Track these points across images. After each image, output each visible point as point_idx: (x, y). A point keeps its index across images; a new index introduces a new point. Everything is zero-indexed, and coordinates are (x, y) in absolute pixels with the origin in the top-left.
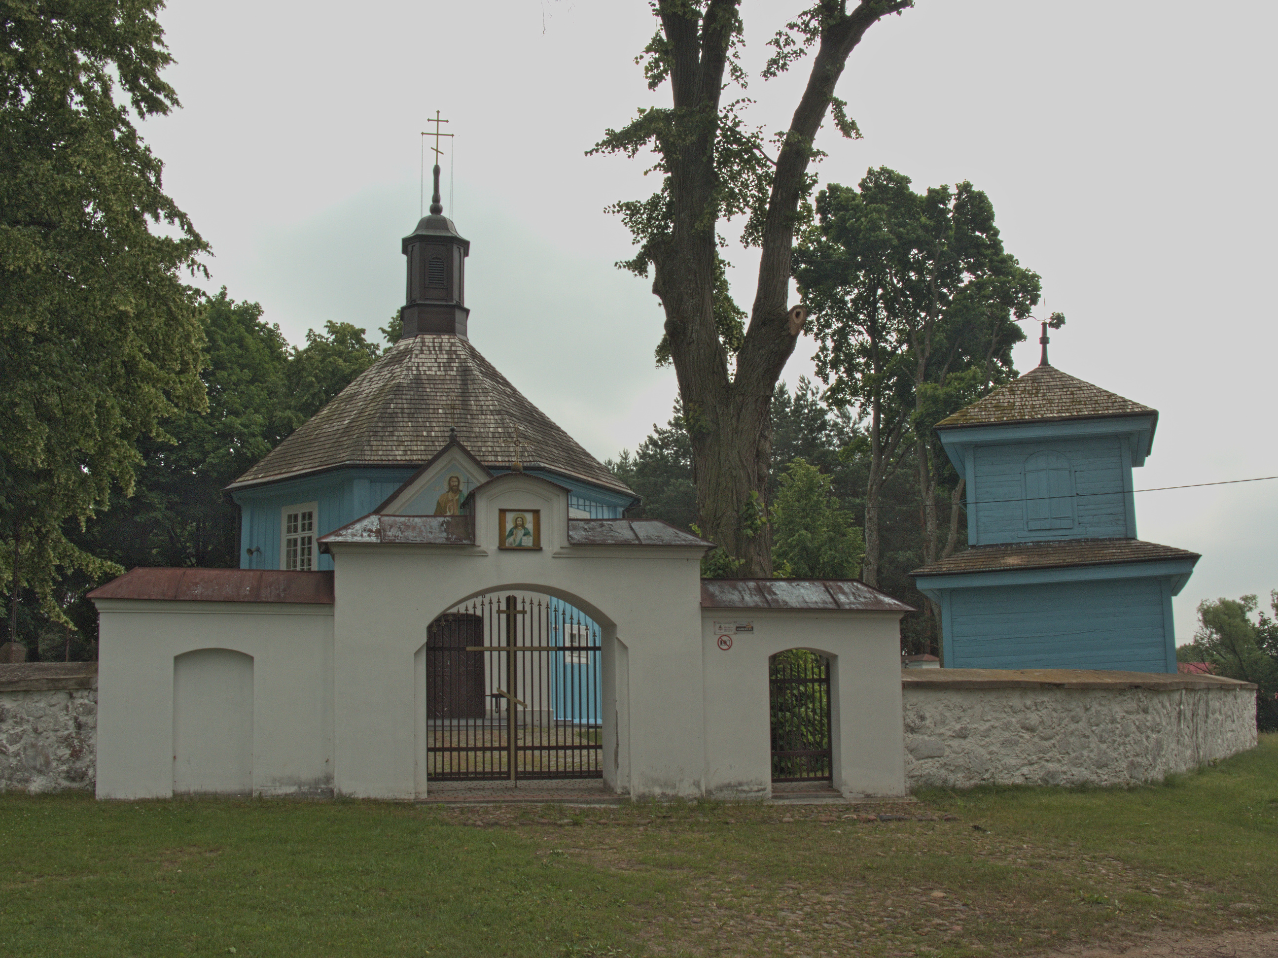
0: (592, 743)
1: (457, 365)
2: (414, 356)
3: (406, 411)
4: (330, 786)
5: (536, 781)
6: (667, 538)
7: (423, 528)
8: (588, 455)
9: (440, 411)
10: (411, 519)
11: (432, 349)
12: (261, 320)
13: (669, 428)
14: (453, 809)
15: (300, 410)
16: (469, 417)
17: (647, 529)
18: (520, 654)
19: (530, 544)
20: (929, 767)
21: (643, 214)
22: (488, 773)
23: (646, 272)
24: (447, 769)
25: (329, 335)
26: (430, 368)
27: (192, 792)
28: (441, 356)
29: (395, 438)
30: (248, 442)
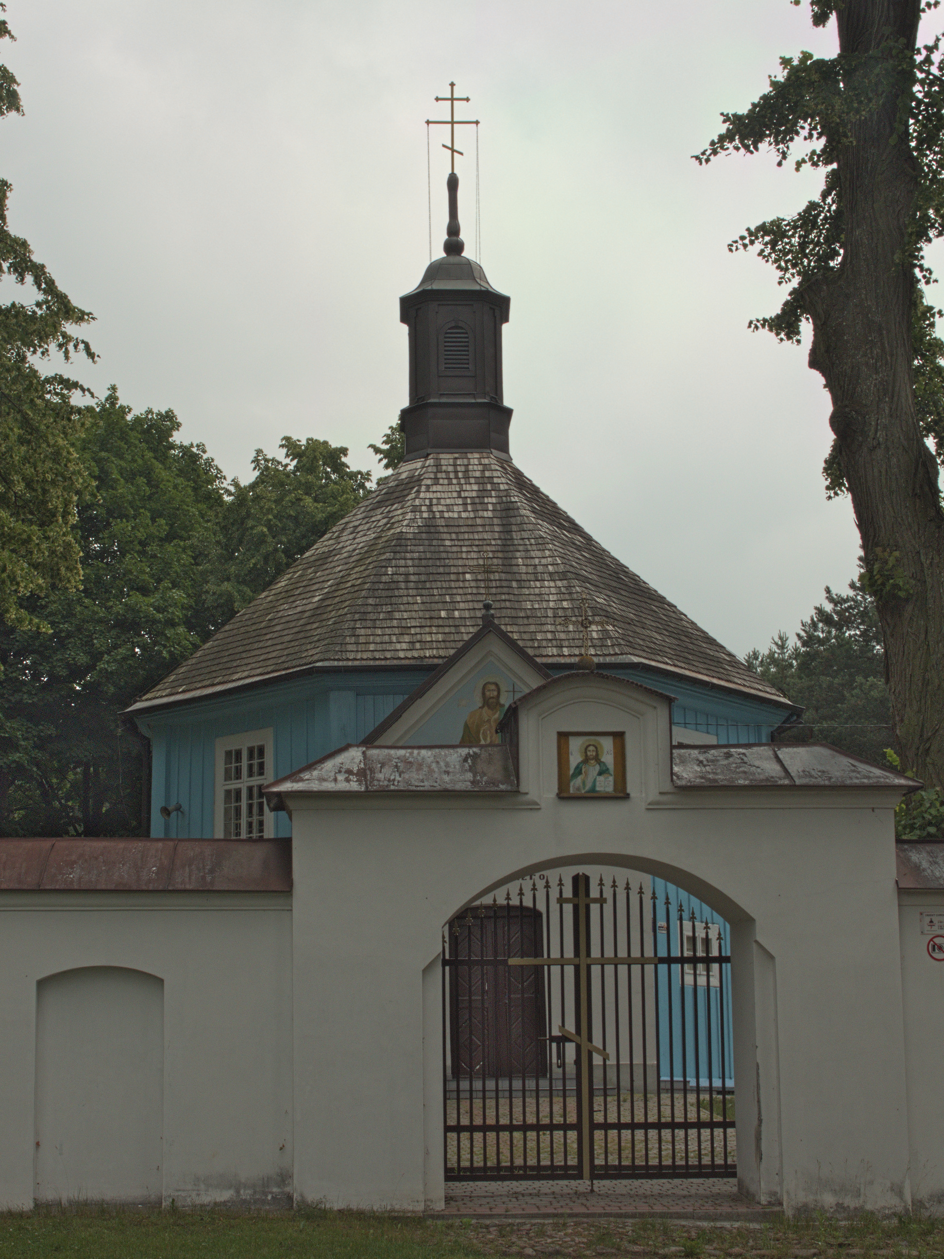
0: (718, 1118)
1: (494, 500)
2: (423, 488)
3: (412, 578)
4: (287, 1189)
5: (625, 1182)
6: (838, 774)
7: (434, 765)
8: (712, 642)
9: (468, 576)
10: (416, 752)
11: (452, 475)
12: (177, 437)
13: (851, 593)
14: (487, 1227)
15: (244, 582)
16: (514, 584)
17: (800, 759)
18: (596, 970)
19: (610, 789)
21: (793, 236)
22: (545, 1168)
23: (798, 333)
24: (478, 1162)
25: (288, 461)
27: (64, 1201)
28: (468, 487)
29: (395, 623)
30: (163, 634)
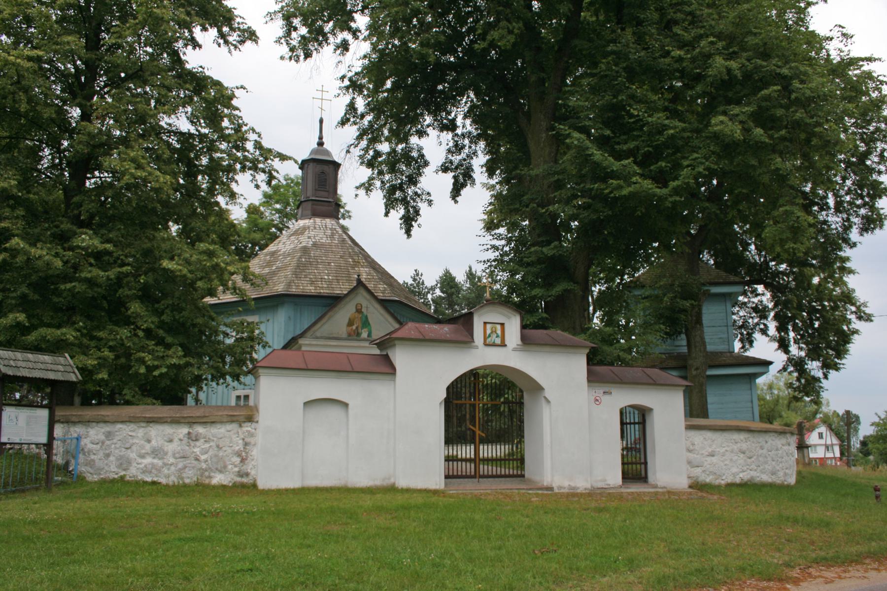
20: (697, 472)
26: (322, 238)
